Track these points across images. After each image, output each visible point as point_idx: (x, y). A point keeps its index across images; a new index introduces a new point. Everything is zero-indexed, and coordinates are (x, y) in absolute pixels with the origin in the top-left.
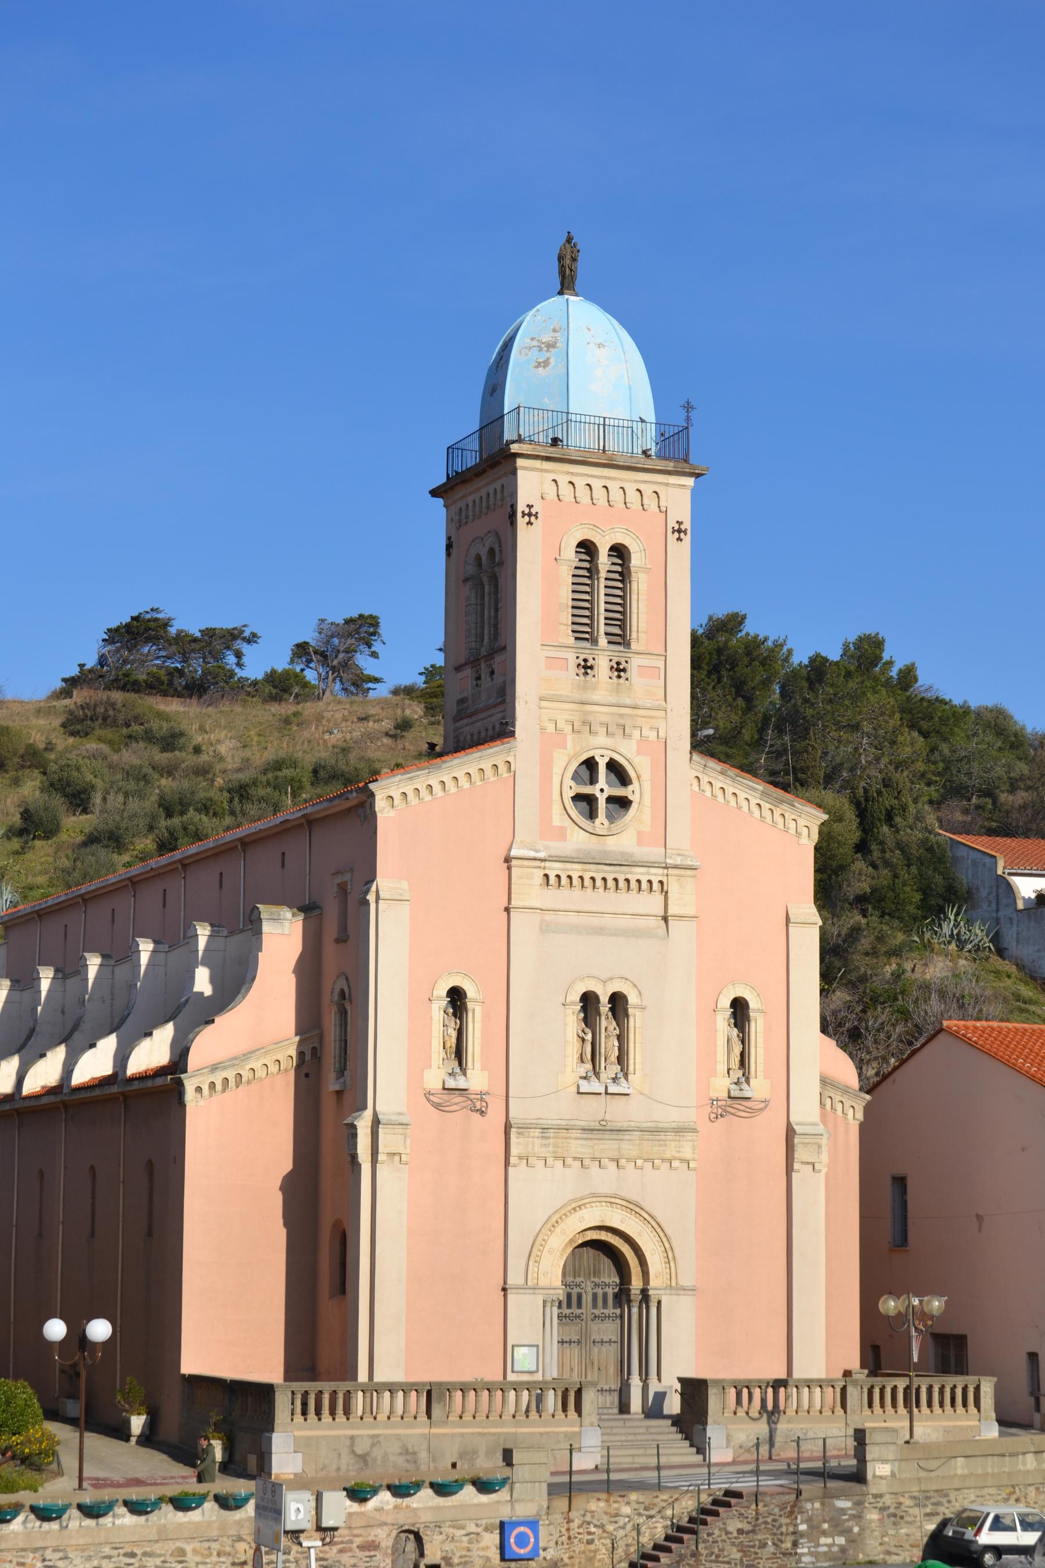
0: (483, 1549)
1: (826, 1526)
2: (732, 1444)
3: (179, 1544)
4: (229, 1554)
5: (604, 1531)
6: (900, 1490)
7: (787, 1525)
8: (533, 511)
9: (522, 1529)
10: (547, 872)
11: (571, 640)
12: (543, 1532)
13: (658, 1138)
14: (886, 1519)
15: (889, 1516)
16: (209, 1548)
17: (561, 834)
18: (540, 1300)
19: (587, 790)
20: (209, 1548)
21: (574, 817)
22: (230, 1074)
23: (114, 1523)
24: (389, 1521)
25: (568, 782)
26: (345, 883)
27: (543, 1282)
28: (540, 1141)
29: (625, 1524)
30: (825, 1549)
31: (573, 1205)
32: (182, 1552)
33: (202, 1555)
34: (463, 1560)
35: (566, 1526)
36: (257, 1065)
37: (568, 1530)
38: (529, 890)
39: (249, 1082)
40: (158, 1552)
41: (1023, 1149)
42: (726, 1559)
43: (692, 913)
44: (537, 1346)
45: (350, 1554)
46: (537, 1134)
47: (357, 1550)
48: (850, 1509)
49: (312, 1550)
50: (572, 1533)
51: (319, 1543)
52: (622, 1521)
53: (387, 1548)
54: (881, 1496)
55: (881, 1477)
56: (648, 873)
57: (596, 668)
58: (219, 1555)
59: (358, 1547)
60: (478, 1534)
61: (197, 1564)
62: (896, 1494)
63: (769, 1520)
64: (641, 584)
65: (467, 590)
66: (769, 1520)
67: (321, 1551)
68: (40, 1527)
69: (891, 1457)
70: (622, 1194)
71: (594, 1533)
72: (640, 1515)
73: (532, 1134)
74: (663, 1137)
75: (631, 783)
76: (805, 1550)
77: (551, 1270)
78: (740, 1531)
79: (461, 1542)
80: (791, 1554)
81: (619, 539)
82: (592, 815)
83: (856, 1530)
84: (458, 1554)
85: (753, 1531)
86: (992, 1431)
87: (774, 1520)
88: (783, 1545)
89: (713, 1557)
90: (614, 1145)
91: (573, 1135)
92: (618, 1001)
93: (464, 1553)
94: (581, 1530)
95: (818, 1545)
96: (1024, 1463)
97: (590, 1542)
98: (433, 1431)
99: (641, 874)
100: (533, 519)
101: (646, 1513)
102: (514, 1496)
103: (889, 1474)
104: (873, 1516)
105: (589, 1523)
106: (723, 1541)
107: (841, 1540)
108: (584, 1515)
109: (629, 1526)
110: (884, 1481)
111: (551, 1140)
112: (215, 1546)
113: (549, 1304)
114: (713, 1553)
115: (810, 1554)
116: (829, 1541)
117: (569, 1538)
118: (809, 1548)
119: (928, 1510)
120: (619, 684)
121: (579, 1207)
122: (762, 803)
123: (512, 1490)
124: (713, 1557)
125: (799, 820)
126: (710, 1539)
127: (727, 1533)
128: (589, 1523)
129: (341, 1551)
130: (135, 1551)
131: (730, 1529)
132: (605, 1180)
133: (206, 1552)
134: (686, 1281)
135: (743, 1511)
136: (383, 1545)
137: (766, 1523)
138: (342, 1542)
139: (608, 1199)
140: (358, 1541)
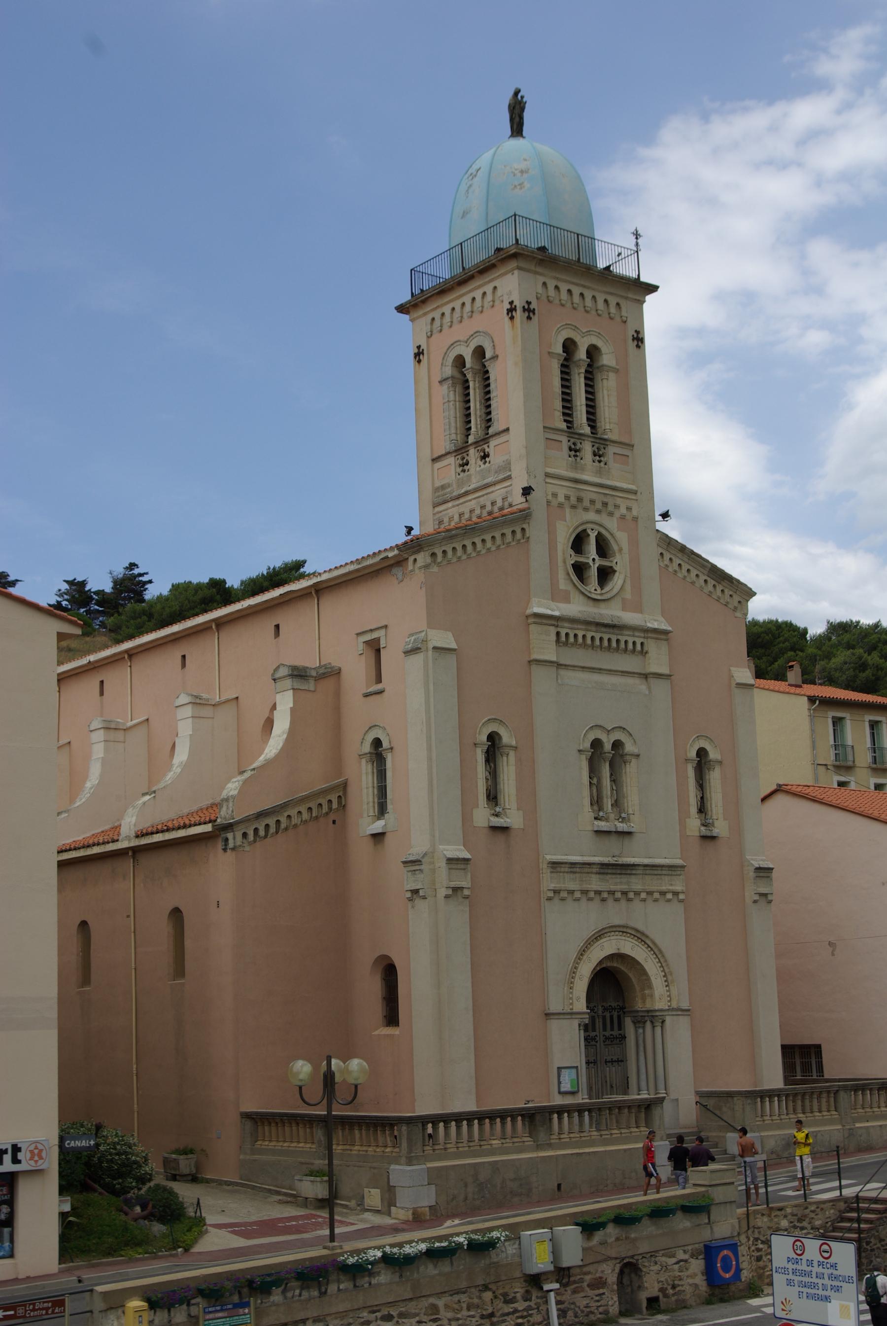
3: (432, 1300)
4: (478, 1307)
9: (725, 1252)
10: (559, 629)
12: (742, 1250)
13: (656, 872)
16: (459, 1301)
17: (567, 600)
18: (576, 1023)
20: (459, 1301)
23: (370, 1284)
24: (614, 1255)
26: (377, 640)
32: (434, 1308)
33: (454, 1310)
39: (286, 829)
40: (413, 1311)
41: (883, 884)
43: (665, 670)
45: (582, 1294)
47: (587, 1289)
53: (613, 1283)
56: (633, 636)
58: (468, 1309)
59: (588, 1286)
60: (686, 1261)
61: (449, 1320)
68: (300, 1295)
75: (614, 555)
81: (595, 341)
92: (617, 745)
99: (629, 635)
102: (711, 1218)
112: (464, 1298)
120: (601, 467)
126: (868, 1247)
129: (575, 1292)
130: (392, 1313)
132: (615, 914)
133: (456, 1306)
136: (609, 1281)
139: (621, 929)
140: (588, 1278)
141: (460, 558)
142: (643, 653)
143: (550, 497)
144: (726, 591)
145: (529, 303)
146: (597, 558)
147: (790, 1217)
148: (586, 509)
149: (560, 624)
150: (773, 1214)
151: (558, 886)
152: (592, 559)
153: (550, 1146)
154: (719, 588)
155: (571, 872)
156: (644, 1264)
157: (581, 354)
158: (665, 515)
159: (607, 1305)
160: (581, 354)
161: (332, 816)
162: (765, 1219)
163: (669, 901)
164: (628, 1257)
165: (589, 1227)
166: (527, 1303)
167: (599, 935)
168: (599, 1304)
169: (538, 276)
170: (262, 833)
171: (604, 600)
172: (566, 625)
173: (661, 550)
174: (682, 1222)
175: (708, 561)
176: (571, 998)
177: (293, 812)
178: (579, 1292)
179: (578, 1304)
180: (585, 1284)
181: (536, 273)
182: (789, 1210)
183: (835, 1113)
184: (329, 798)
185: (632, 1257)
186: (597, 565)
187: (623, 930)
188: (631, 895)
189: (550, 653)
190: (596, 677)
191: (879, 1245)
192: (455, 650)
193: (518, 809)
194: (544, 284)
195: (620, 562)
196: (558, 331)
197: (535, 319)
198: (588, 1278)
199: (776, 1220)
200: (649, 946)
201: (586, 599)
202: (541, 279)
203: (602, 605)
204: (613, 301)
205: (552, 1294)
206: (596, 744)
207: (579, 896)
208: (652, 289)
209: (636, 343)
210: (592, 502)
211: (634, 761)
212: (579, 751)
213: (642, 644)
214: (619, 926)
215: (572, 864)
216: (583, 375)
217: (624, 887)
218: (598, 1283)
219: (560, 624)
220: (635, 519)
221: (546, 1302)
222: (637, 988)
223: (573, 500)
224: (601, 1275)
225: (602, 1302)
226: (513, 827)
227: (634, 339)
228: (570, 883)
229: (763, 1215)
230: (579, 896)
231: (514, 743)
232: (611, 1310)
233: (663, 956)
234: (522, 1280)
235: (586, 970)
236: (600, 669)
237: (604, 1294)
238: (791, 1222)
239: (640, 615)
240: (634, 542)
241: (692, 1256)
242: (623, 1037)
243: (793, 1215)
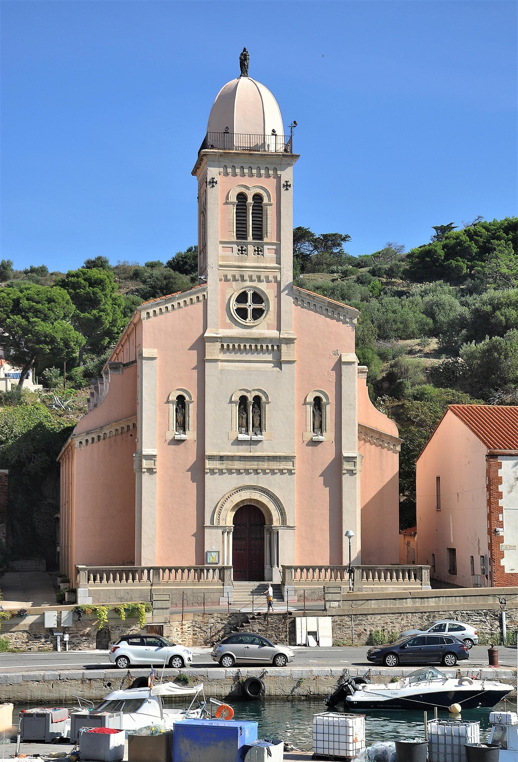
8: (289, 183)
19: (242, 306)
22: (95, 436)
25: (233, 302)
36: (107, 432)
38: (213, 351)
44: (219, 552)
50: (184, 630)
64: (271, 212)
77: (229, 522)
78: (260, 630)
82: (245, 317)
85: (266, 630)
86: (427, 588)
88: (281, 637)
90: (256, 463)
92: (257, 399)
94: (190, 629)
96: (406, 603)
98: (153, 588)
105: (194, 626)
117: (182, 632)
119: (356, 623)
120: (258, 257)
122: (328, 308)
131: (254, 629)
137: (272, 627)
157: (250, 200)
160: (250, 200)
171: (255, 326)
186: (252, 308)
206: (243, 400)
217: (255, 467)
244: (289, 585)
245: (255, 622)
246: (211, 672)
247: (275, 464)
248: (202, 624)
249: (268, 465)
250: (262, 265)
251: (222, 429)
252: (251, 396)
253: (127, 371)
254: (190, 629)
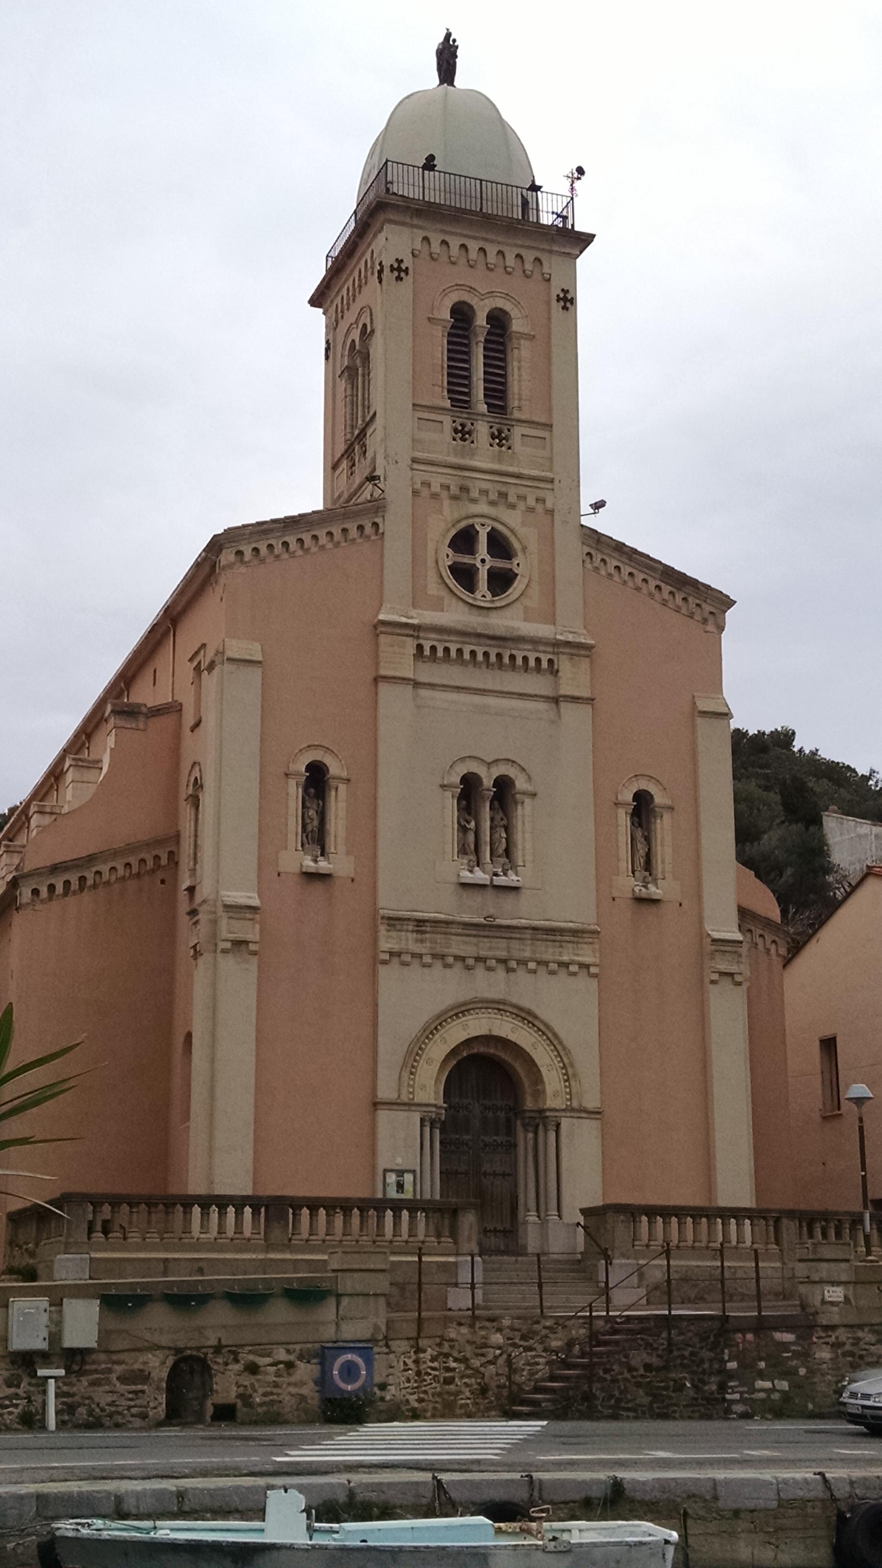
0: (295, 1385)
1: (762, 1365)
2: (645, 1283)
5: (468, 1367)
6: (857, 1321)
7: (711, 1360)
9: (349, 1356)
11: (448, 404)
14: (841, 1359)
15: (844, 1355)
17: (438, 605)
18: (416, 1117)
21: (451, 586)
24: (164, 1343)
27: (421, 1097)
28: (415, 935)
29: (496, 1357)
30: (762, 1395)
31: (456, 1011)
34: (267, 1399)
35: (414, 1357)
37: (417, 1362)
39: (95, 886)
42: (630, 1405)
43: (585, 693)
44: (414, 1171)
46: (411, 928)
48: (793, 1343)
49: (52, 1382)
50: (422, 1367)
51: (62, 1372)
52: (491, 1353)
54: (833, 1328)
55: (832, 1303)
57: (474, 435)
62: (852, 1326)
63: (687, 1353)
65: (342, 384)
66: (687, 1353)
67: (65, 1384)
69: (844, 1278)
70: (514, 1000)
71: (454, 1369)
72: (515, 1345)
73: (405, 927)
74: (559, 938)
75: (516, 555)
76: (737, 1396)
77: (429, 1087)
78: (648, 1367)
79: (266, 1373)
80: (716, 1399)
83: (802, 1371)
84: (261, 1391)
87: (692, 1354)
88: (707, 1388)
89: (613, 1402)
90: (503, 943)
91: (453, 931)
92: (503, 785)
93: (269, 1389)
94: (435, 1364)
95: (753, 1390)
97: (449, 1381)
100: (403, 275)
101: (522, 1343)
102: (340, 1312)
103: (842, 1299)
104: (824, 1354)
105: (447, 1355)
106: (626, 1379)
107: (784, 1385)
108: (440, 1345)
109: (501, 1361)
110: (835, 1309)
111: (428, 936)
113: (427, 1123)
114: (612, 1396)
115: (742, 1401)
116: (768, 1384)
117: (418, 1373)
118: (741, 1393)
121: (462, 1012)
123: (338, 1305)
124: (613, 1402)
125: (704, 605)
126: (608, 1377)
127: (631, 1369)
128: (447, 1355)
129: (93, 1384)
131: (633, 1363)
132: (489, 984)
134: (592, 1102)
135: (650, 1339)
137: (683, 1357)
138: (96, 1371)
139: (496, 1006)
140: (119, 1369)
141: (277, 557)
142: (553, 670)
143: (418, 486)
144: (690, 599)
145: (565, 308)
146: (488, 558)
147: (507, 1331)
148: (474, 501)
149: (422, 634)
150: (478, 1325)
151: (396, 948)
152: (482, 561)
153: (288, 1246)
154: (679, 597)
155: (417, 931)
156: (216, 1363)
157: (481, 320)
158: (598, 506)
159: (146, 1407)
160: (481, 320)
161: (160, 875)
162: (464, 1330)
163: (574, 974)
164: (190, 1349)
165: (116, 1303)
166: (13, 1390)
167: (460, 1010)
168: (132, 1403)
169: (415, 230)
170: (60, 889)
171: (496, 608)
172: (433, 636)
173: (587, 549)
174: (280, 1313)
175: (660, 562)
176: (413, 1087)
177: (105, 868)
178: (100, 1385)
179: (96, 1400)
180: (114, 1377)
181: (412, 226)
182: (506, 1322)
183: (775, 1246)
184: (156, 852)
185: (198, 1349)
186: (487, 567)
187: (499, 1006)
188: (513, 964)
189: (406, 668)
190: (477, 699)
191: (628, 1376)
192: (260, 662)
193: (348, 853)
194: (426, 239)
195: (524, 565)
196: (445, 293)
197: (408, 280)
198: (119, 1369)
199: (483, 1333)
200: (539, 1030)
201: (467, 609)
202: (421, 233)
203: (494, 614)
204: (529, 256)
205: (52, 1382)
206: (470, 782)
207: (430, 961)
208: (586, 240)
209: (562, 303)
210: (484, 492)
211: (527, 801)
212: (443, 786)
213: (550, 661)
214: (493, 1002)
215: (419, 921)
216: (482, 345)
217: (502, 954)
218: (142, 1377)
219: (422, 634)
220: (551, 512)
221: (45, 1392)
222: (526, 1083)
223: (454, 490)
224: (141, 1367)
225: (138, 1402)
226: (335, 875)
227: (559, 299)
228: (408, 941)
229: (460, 1324)
230: (430, 961)
231: (344, 774)
232: (151, 1414)
233: (561, 1043)
234: (8, 1360)
235: (438, 1050)
236: (485, 690)
237: (143, 1392)
238: (509, 1339)
239: (552, 627)
240: (549, 540)
241: (301, 1357)
242: (515, 1146)
243: (513, 1329)
244: (623, 1256)
245: (635, 1340)
246: (727, 1482)
247: (551, 950)
248: (469, 1348)
249: (534, 952)
250: (511, 469)
251: (416, 858)
252: (490, 776)
253: (156, 724)
254: (435, 1364)
